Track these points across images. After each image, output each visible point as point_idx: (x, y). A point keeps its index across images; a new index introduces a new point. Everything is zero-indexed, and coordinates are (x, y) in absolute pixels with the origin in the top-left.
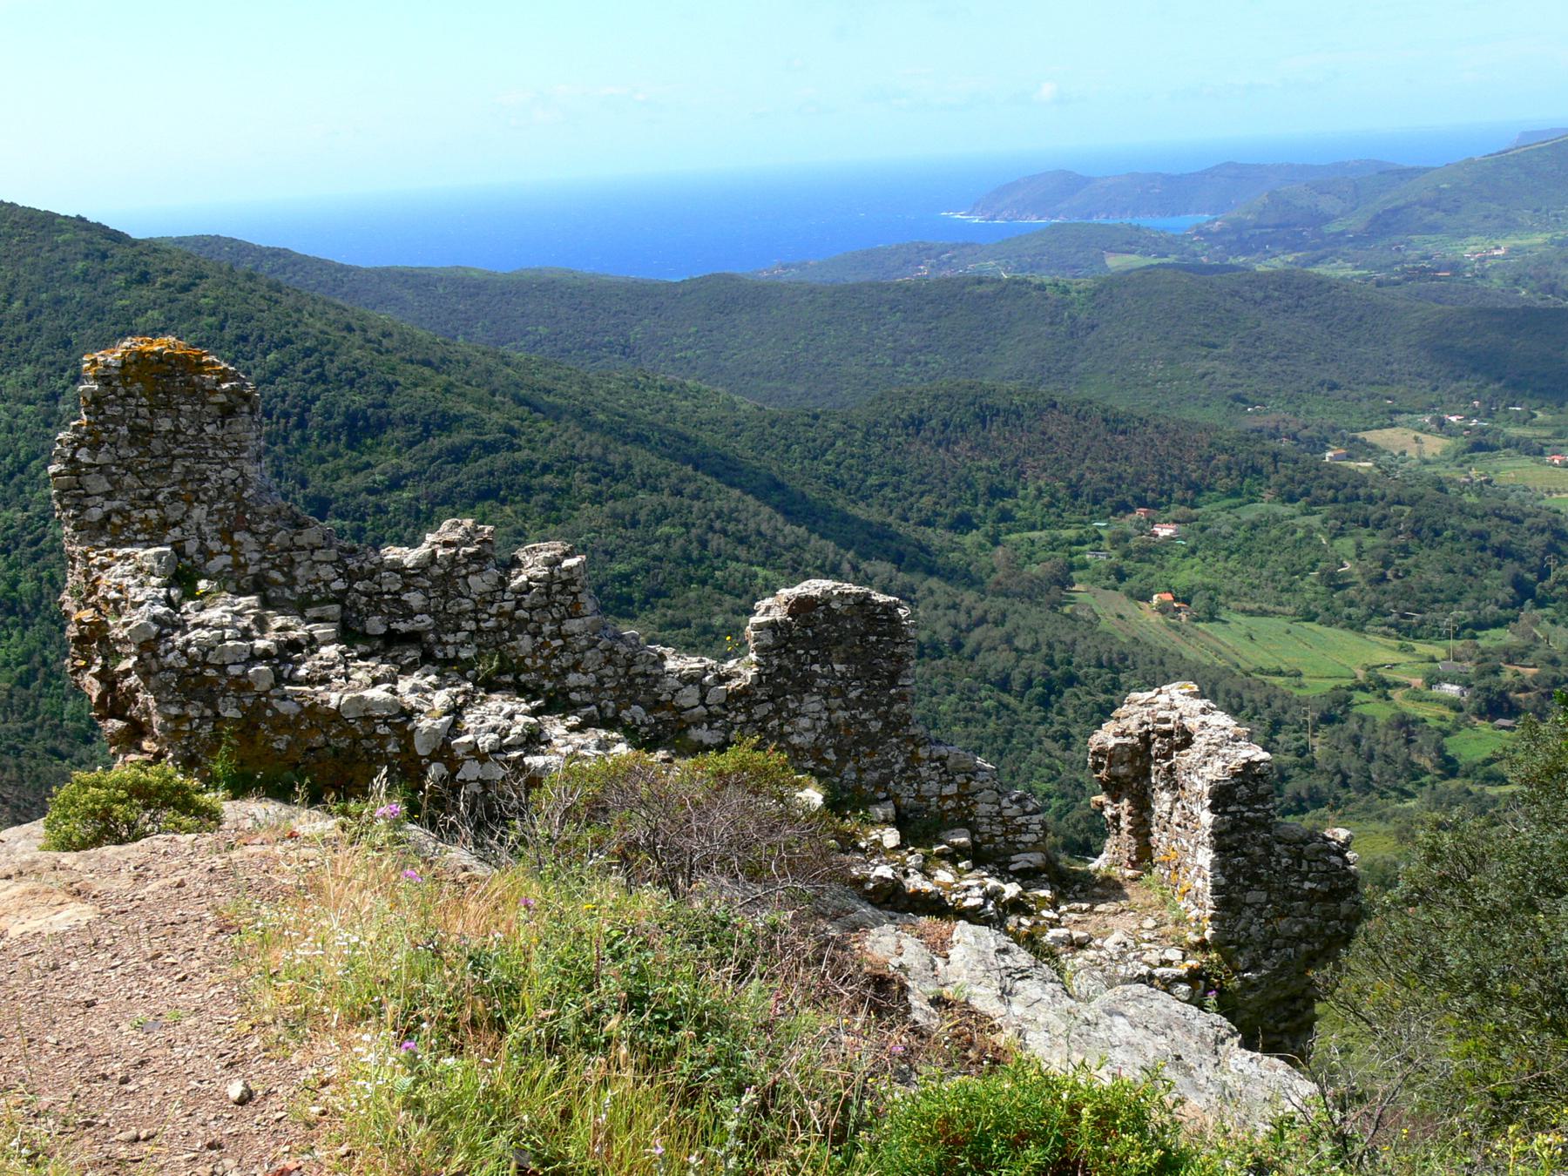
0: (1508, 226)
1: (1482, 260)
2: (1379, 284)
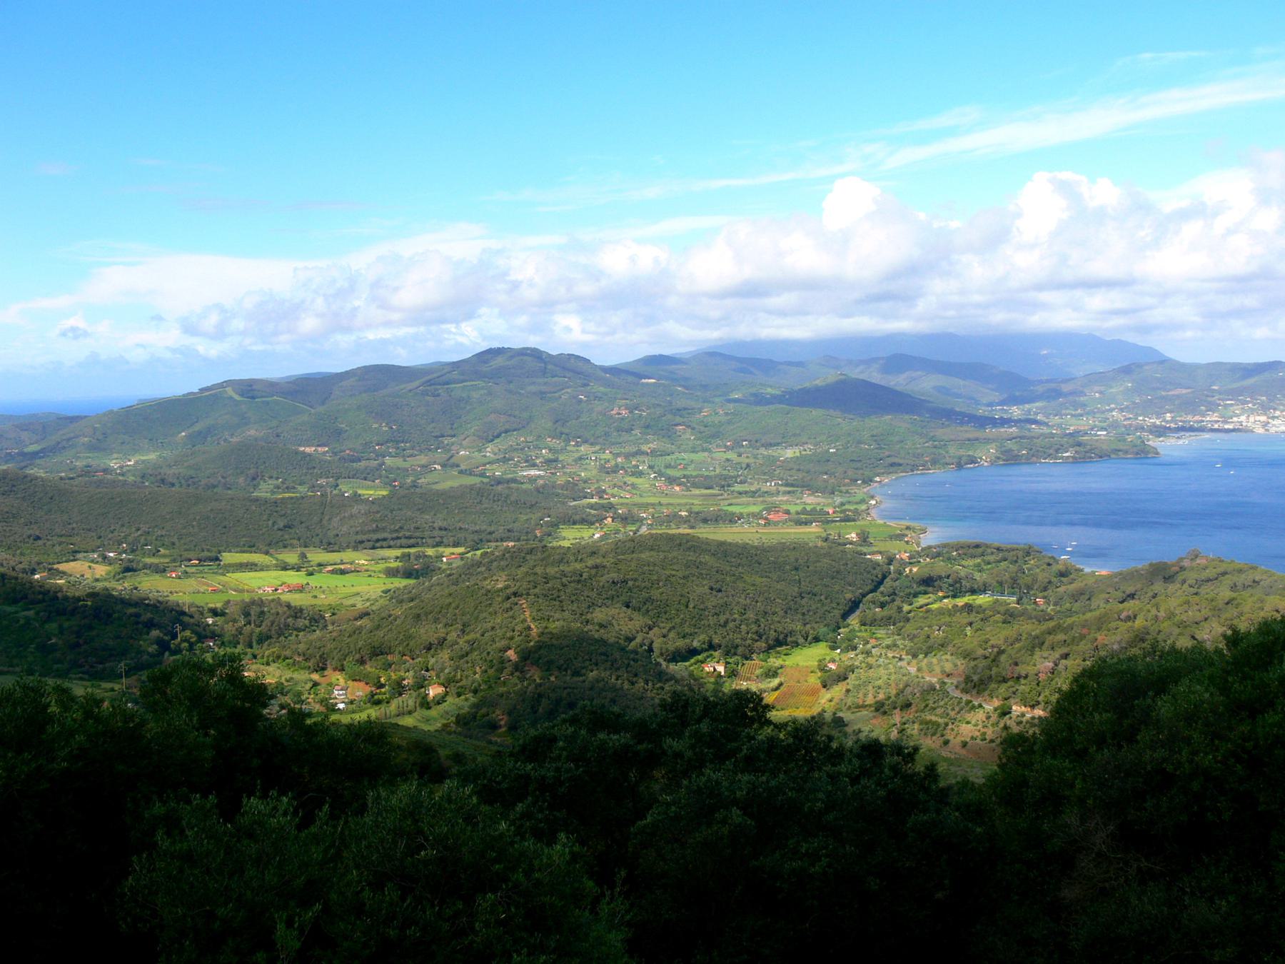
0: (135, 450)
1: (121, 467)
2: (61, 478)
